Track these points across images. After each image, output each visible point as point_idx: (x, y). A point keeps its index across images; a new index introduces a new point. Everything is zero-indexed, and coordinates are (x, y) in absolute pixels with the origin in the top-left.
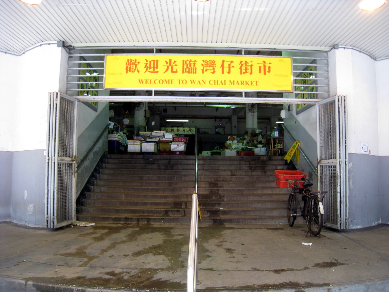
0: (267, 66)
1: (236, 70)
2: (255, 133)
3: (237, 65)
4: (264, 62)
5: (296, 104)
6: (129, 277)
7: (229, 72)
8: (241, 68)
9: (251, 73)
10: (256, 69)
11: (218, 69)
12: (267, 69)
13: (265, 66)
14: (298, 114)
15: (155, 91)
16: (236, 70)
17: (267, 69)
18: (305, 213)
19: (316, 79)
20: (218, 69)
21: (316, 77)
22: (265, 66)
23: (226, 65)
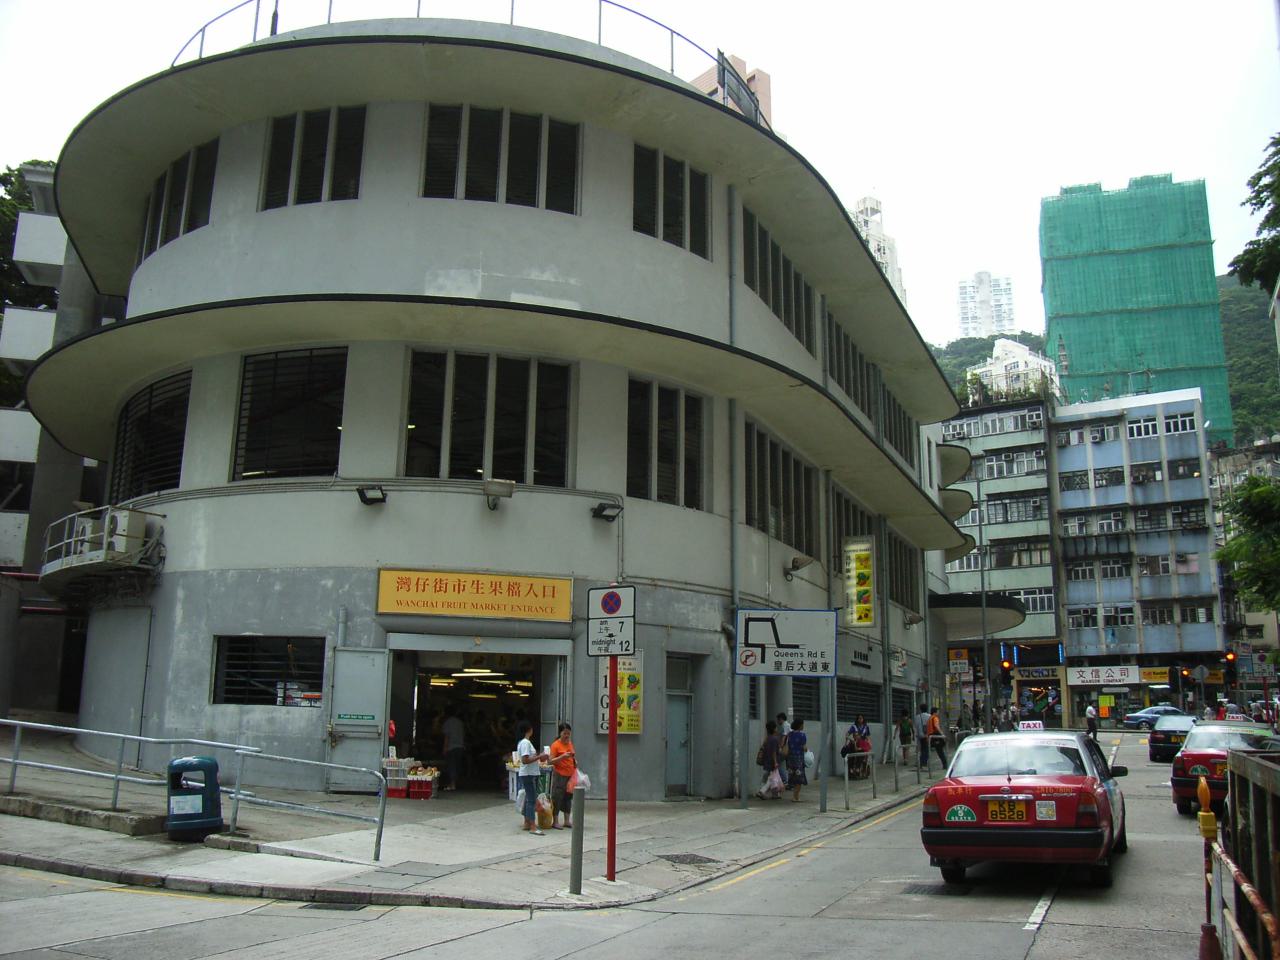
0: (462, 584)
1: (430, 589)
2: (1112, 708)
3: (431, 583)
4: (459, 580)
5: (297, 105)
6: (1244, 746)
7: (424, 590)
8: (435, 586)
9: (446, 592)
10: (450, 588)
11: (413, 587)
12: (462, 588)
13: (459, 585)
14: (746, 428)
15: (1168, 564)
16: (430, 589)
17: (462, 588)
18: (21, 489)
19: (1165, 466)
20: (413, 587)
21: (1160, 469)
22: (459, 585)
23: (421, 582)
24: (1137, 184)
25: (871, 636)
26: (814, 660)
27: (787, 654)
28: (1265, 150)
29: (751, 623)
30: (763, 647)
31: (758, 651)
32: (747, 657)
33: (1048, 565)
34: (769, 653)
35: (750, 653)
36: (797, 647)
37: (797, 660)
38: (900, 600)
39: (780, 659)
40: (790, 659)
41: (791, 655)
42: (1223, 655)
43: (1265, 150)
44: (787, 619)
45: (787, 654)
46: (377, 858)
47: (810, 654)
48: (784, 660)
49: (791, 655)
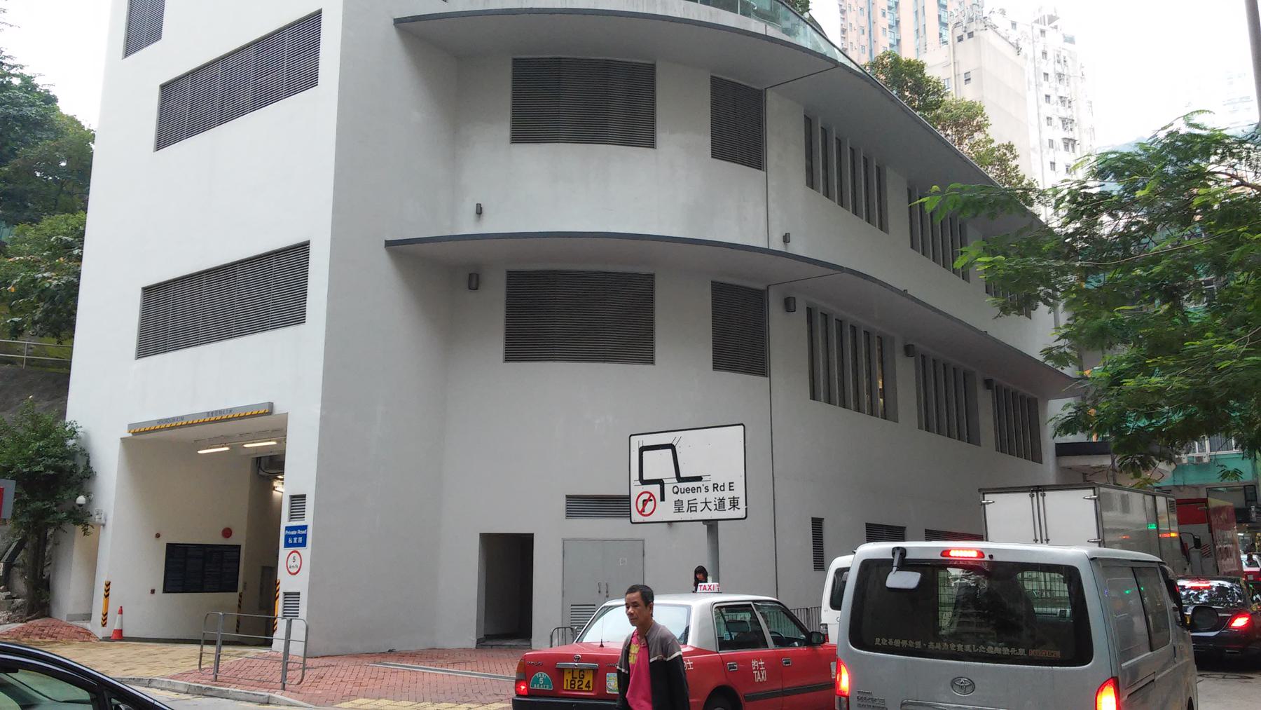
24: (72, 120)
25: (736, 496)
26: (720, 494)
27: (687, 490)
28: (607, 585)
29: (645, 453)
30: (660, 482)
31: (655, 489)
32: (645, 502)
33: (945, 604)
34: (668, 488)
35: (646, 496)
36: (699, 479)
37: (700, 497)
38: (848, 330)
39: (680, 496)
40: (691, 496)
41: (693, 490)
42: (619, 672)
43: (607, 585)
44: (1014, 24)
45: (687, 490)
46: (711, 510)
47: (715, 487)
48: (685, 498)
49: (693, 490)
